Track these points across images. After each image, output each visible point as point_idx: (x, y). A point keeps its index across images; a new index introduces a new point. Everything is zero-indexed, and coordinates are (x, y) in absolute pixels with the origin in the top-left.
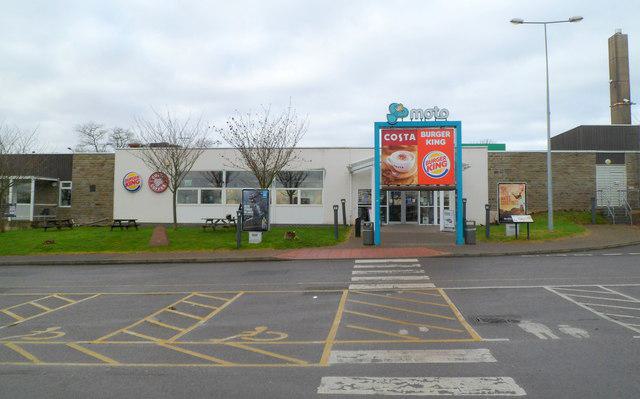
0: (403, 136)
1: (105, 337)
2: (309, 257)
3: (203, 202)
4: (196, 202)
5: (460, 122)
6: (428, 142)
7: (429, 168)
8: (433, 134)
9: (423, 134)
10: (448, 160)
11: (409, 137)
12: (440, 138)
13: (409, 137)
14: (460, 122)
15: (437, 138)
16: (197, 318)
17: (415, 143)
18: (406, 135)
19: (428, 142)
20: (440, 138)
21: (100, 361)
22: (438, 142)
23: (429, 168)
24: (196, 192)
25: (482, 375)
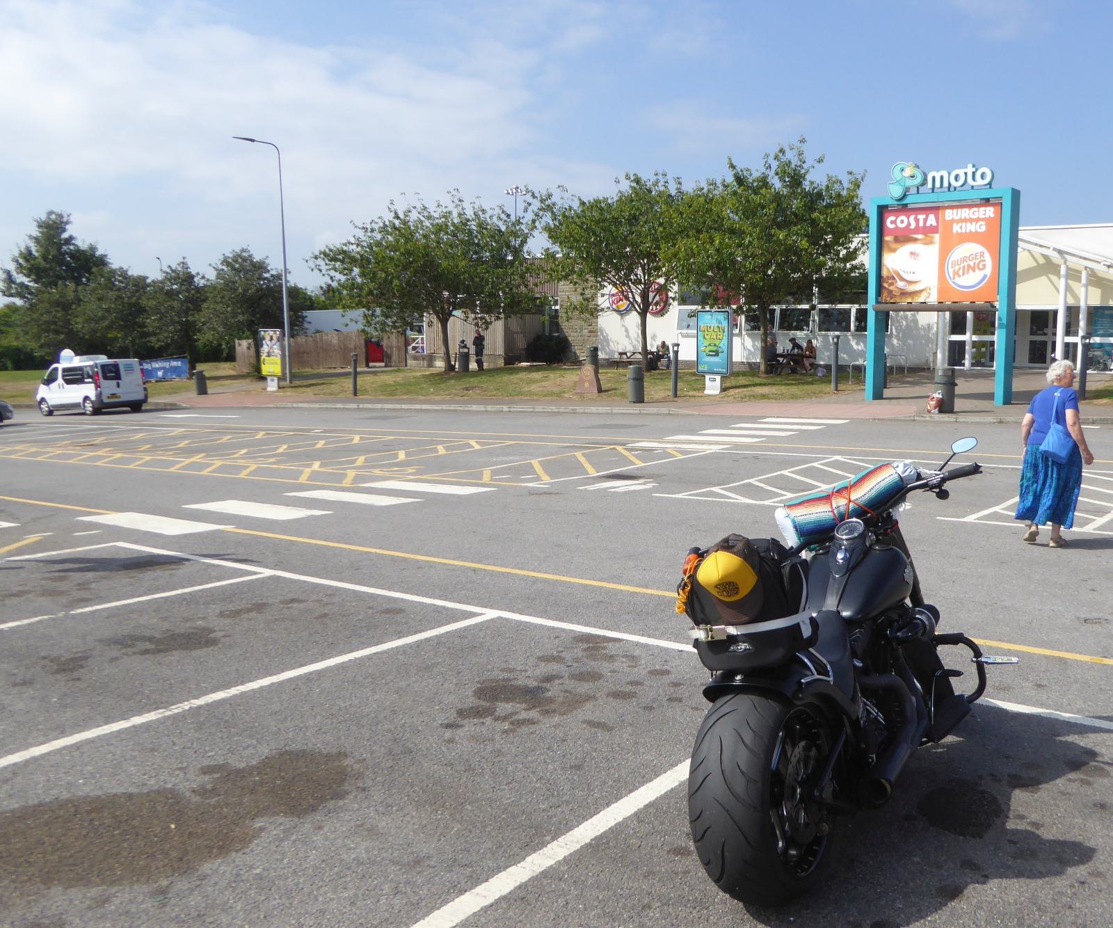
0: (917, 220)
1: (183, 464)
2: (623, 423)
3: (1032, 342)
4: (1032, 333)
5: (878, 206)
6: (956, 228)
7: (956, 273)
8: (965, 213)
9: (949, 214)
10: (988, 257)
11: (925, 221)
12: (977, 220)
13: (925, 221)
14: (878, 206)
15: (971, 220)
16: (321, 470)
17: (934, 230)
18: (921, 217)
19: (956, 228)
20: (977, 220)
21: (255, 573)
22: (971, 227)
23: (956, 273)
24: (848, 312)
25: (1032, 785)
